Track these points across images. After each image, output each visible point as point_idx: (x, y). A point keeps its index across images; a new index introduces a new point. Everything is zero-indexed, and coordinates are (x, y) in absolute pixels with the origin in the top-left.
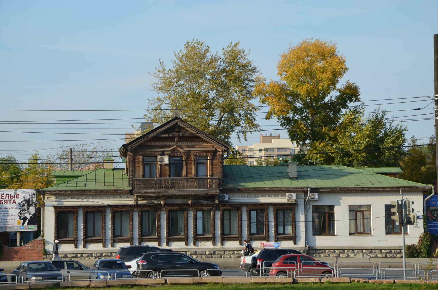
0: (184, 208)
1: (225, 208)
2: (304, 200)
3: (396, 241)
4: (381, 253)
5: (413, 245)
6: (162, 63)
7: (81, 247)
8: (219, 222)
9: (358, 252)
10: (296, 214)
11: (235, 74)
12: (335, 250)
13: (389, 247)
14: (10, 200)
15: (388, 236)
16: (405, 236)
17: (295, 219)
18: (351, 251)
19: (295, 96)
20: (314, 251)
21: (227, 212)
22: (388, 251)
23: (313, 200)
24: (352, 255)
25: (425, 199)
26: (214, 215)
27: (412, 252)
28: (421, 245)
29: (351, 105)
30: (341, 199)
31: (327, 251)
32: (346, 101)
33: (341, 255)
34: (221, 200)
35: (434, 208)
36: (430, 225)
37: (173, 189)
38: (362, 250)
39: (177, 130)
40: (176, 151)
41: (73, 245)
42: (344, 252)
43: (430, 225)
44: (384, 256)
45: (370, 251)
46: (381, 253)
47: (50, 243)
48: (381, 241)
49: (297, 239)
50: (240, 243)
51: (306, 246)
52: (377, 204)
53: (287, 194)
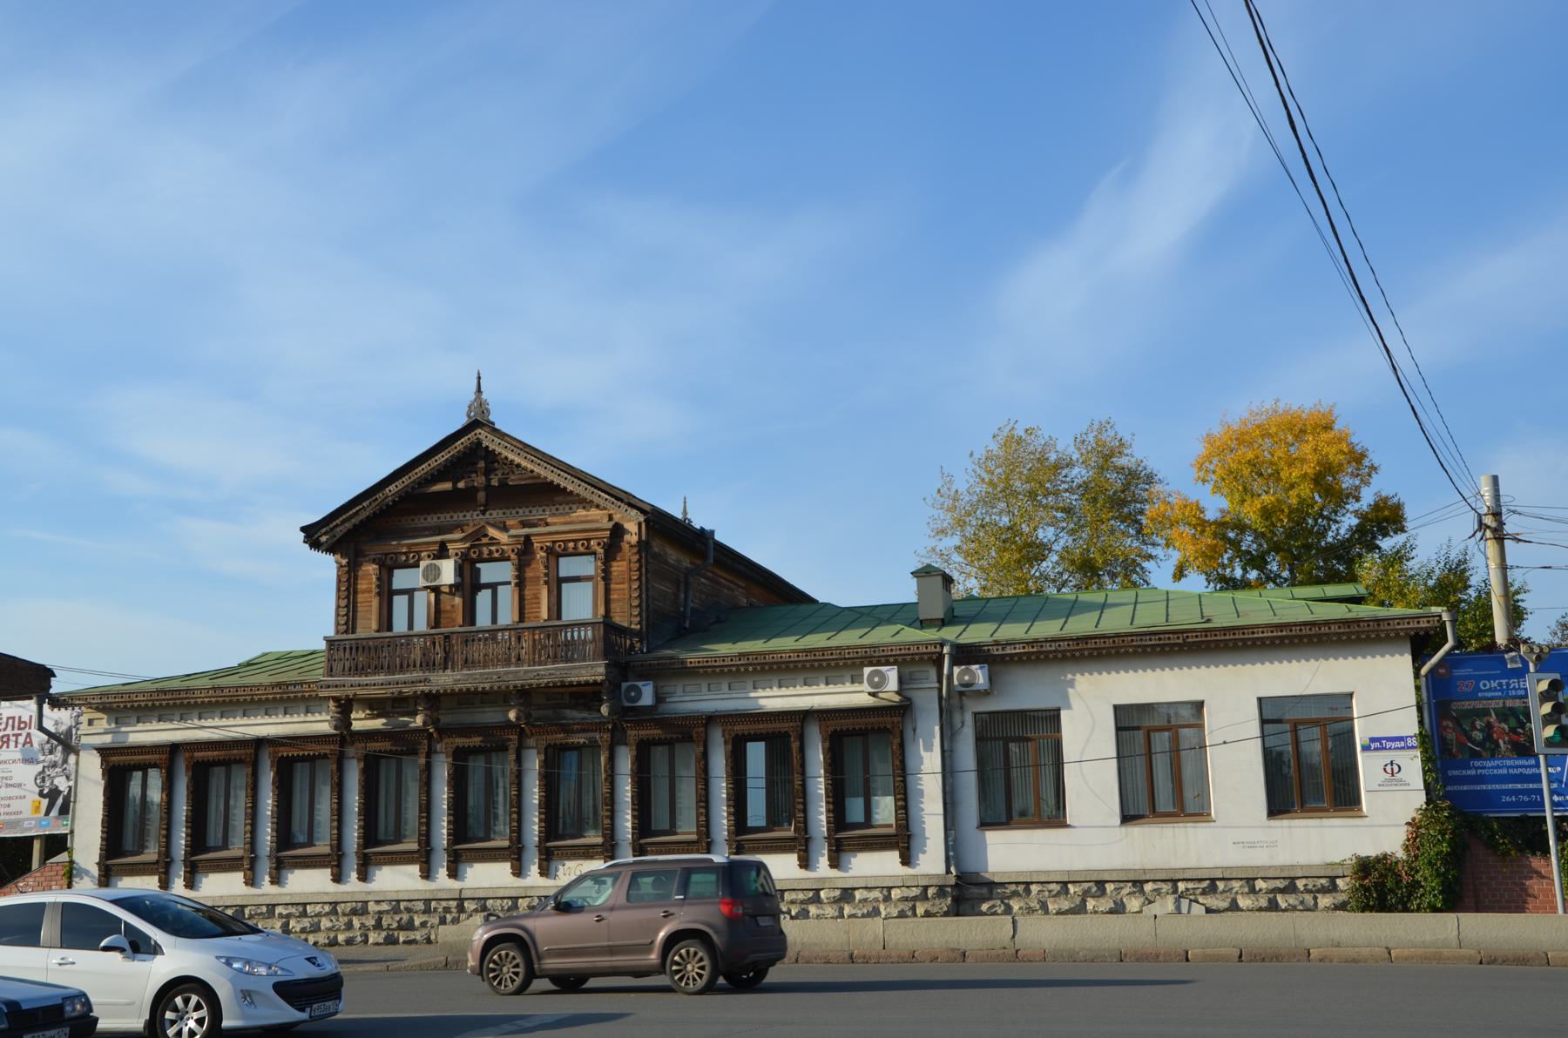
0: (496, 742)
1: (646, 733)
2: (935, 694)
3: (1323, 843)
4: (1253, 891)
5: (1385, 856)
6: (950, 480)
7: (178, 887)
8: (629, 788)
9: (1158, 891)
10: (909, 748)
11: (1119, 495)
12: (1065, 884)
13: (1282, 868)
14: (17, 736)
15: (1275, 823)
16: (1189, 811)
17: (903, 762)
18: (1128, 888)
19: (1241, 527)
20: (985, 891)
21: (660, 748)
22: (1280, 884)
23: (967, 692)
24: (1133, 904)
25: (1424, 671)
26: (612, 759)
27: (1378, 886)
28: (1416, 857)
29: (1386, 544)
30: (1072, 684)
31: (1034, 888)
32: (1374, 538)
33: (1091, 904)
34: (627, 704)
35: (1467, 705)
36: (1456, 773)
37: (449, 672)
38: (1175, 882)
39: (482, 464)
40: (485, 540)
41: (328, 871)
42: (1104, 890)
43: (1456, 773)
44: (1264, 903)
45: (1205, 884)
46: (1253, 891)
47: (87, 873)
48: (1252, 845)
49: (915, 843)
50: (901, 856)
51: (948, 872)
52: (1230, 701)
53: (867, 670)
